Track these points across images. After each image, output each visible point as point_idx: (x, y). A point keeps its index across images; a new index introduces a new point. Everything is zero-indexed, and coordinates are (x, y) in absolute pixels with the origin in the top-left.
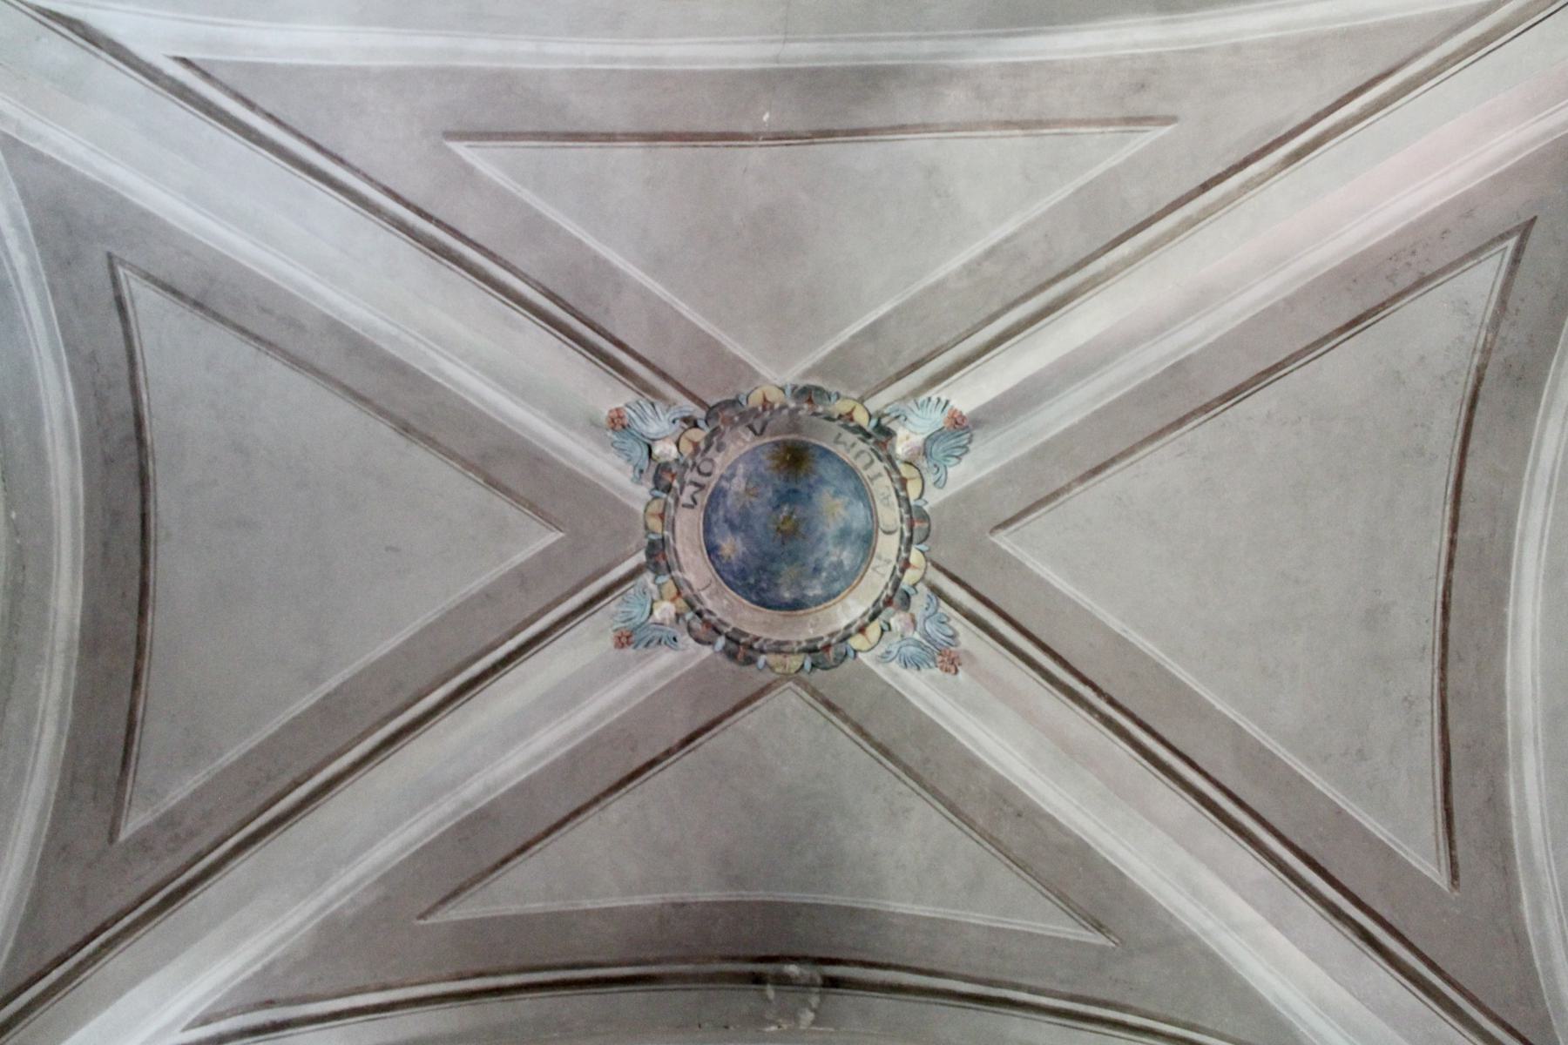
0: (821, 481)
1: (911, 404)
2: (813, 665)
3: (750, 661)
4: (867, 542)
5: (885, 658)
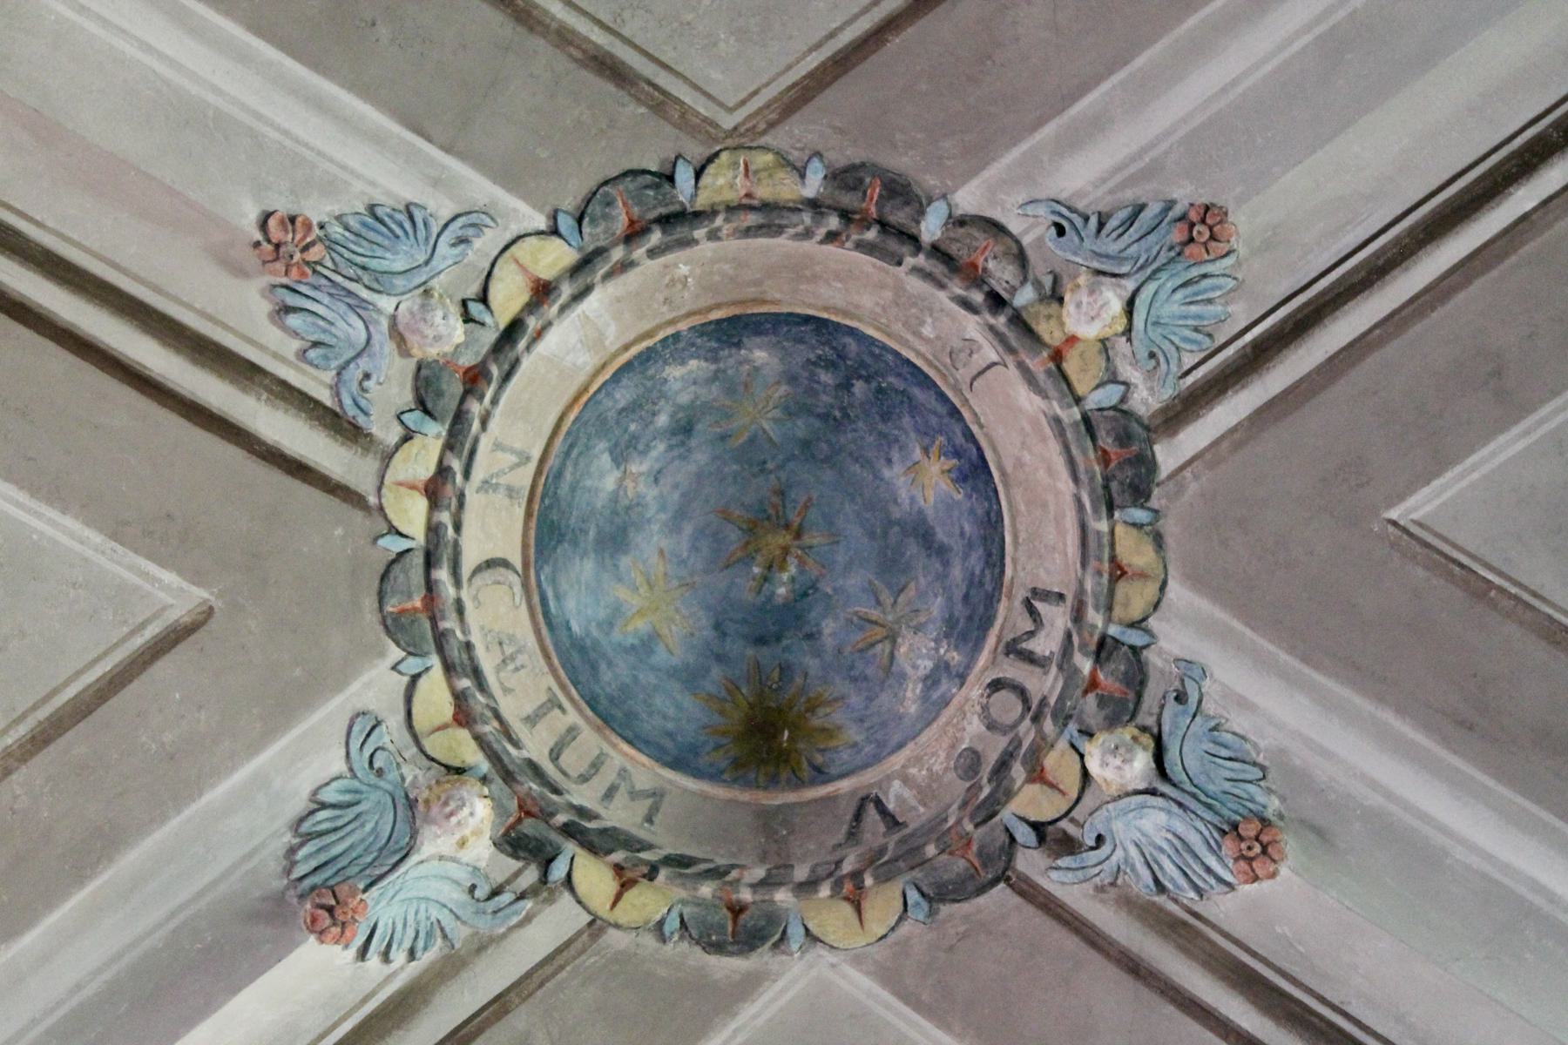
0: (689, 677)
1: (460, 934)
2: (671, 179)
3: (846, 177)
4: (549, 528)
5: (469, 222)
